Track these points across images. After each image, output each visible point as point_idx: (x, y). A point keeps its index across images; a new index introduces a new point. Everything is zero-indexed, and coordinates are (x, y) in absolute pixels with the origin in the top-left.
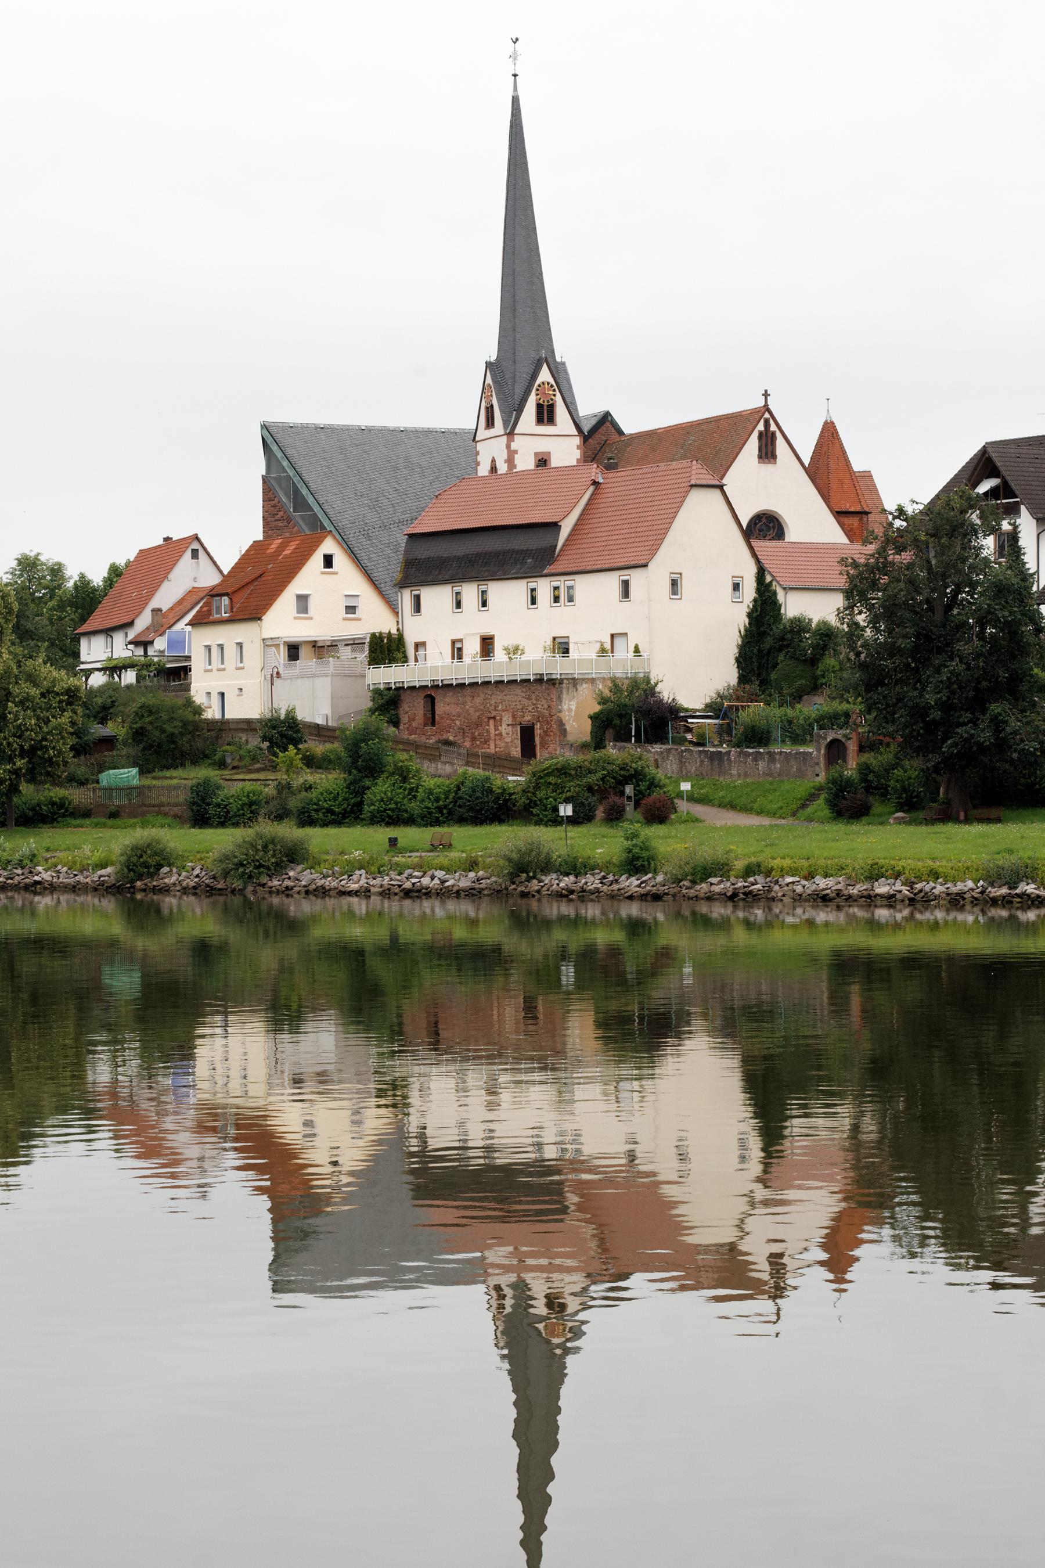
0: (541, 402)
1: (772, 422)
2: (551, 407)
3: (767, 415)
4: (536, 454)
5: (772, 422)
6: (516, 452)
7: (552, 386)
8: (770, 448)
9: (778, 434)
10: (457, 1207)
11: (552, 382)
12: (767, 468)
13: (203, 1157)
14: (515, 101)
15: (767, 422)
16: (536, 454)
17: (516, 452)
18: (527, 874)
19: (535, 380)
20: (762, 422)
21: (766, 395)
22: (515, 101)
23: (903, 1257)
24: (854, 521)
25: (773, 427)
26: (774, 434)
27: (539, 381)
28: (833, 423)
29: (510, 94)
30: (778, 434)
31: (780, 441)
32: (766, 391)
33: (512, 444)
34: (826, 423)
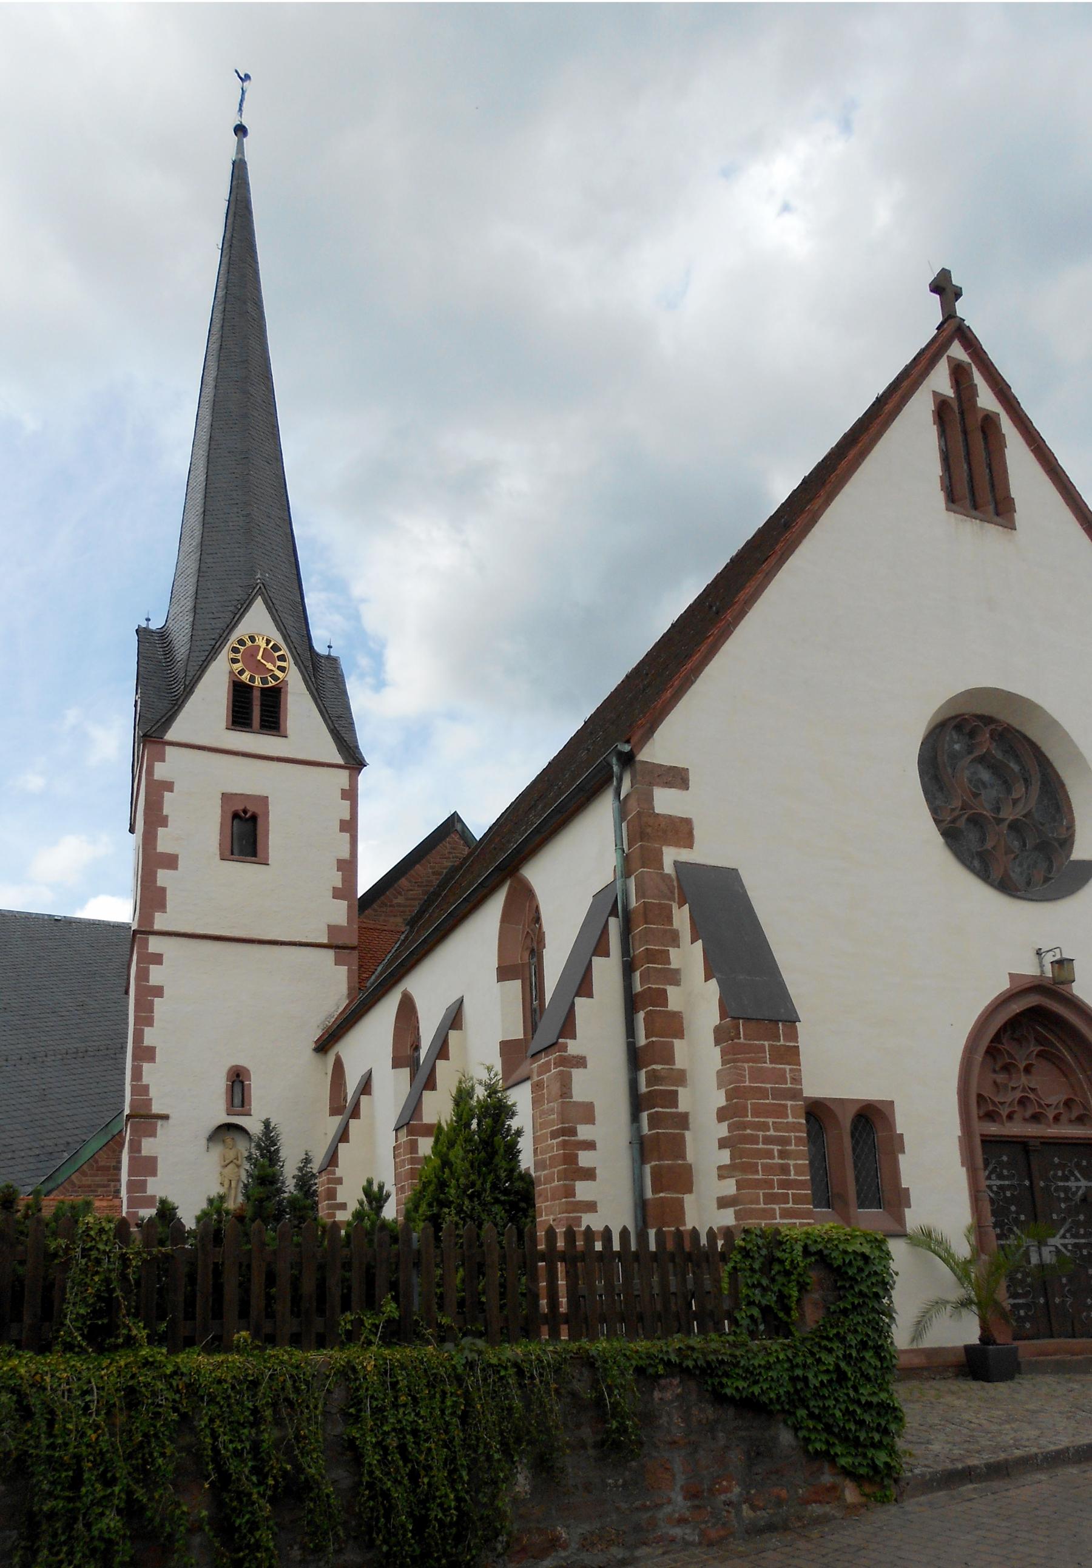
0: (245, 677)
1: (978, 379)
2: (273, 698)
3: (957, 351)
4: (226, 797)
5: (978, 379)
9: (1007, 426)
13: (430, 1399)
14: (239, 169)
15: (959, 373)
16: (226, 797)
18: (411, 1531)
19: (231, 627)
21: (944, 287)
22: (239, 169)
23: (460, 1082)
26: (989, 422)
27: (242, 631)
29: (232, 155)
30: (1007, 426)
31: (1016, 454)
32: (945, 274)
33: (158, 767)
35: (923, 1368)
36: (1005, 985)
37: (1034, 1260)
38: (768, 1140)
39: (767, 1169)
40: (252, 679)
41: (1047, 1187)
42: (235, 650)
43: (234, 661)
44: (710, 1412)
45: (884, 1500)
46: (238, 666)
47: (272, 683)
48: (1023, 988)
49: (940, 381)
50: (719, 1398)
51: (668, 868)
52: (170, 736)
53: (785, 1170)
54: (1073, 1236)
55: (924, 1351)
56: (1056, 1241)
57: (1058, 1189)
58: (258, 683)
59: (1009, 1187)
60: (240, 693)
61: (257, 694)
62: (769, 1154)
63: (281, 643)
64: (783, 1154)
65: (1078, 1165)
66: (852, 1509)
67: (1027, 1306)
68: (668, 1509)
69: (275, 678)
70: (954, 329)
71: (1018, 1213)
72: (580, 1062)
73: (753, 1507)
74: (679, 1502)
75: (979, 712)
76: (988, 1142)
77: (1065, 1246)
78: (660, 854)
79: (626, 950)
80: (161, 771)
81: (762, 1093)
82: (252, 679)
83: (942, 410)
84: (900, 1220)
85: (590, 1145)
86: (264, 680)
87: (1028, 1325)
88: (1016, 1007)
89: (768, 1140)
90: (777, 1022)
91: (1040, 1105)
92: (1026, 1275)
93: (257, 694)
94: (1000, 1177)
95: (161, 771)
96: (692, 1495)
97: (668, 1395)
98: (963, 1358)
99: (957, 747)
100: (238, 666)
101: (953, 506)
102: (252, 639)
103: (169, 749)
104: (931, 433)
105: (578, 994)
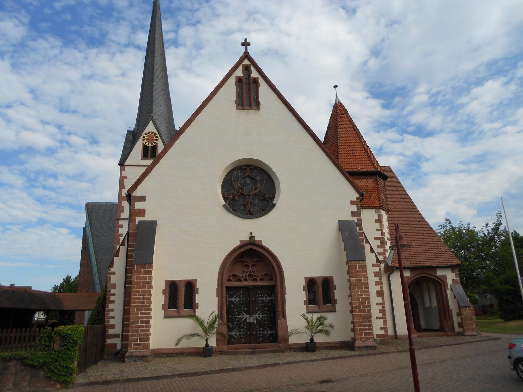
0: (146, 144)
1: (252, 69)
5: (252, 69)
6: (125, 177)
7: (155, 134)
8: (253, 94)
9: (261, 80)
10: (432, 275)
11: (155, 131)
12: (248, 116)
15: (247, 69)
17: (125, 177)
20: (241, 68)
24: (368, 183)
25: (254, 74)
26: (255, 81)
27: (146, 131)
28: (341, 104)
30: (261, 80)
32: (246, 40)
34: (336, 104)
35: (194, 353)
36: (238, 244)
37: (248, 321)
38: (139, 295)
39: (138, 302)
40: (148, 144)
41: (255, 300)
42: (144, 137)
43: (144, 140)
44: (23, 368)
45: (66, 388)
46: (145, 141)
47: (154, 144)
48: (243, 244)
49: (239, 72)
50: (26, 365)
51: (137, 223)
52: (125, 164)
53: (143, 302)
54: (262, 314)
55: (179, 349)
56: (257, 315)
57: (259, 300)
58: (150, 145)
59: (242, 300)
60: (145, 148)
61: (150, 148)
62: (139, 299)
63: (157, 133)
64: (143, 298)
65: (267, 293)
66: (59, 389)
67: (243, 335)
68: (8, 387)
69: (155, 143)
70: (246, 56)
71: (244, 308)
72: (114, 273)
73: (30, 387)
74: (10, 385)
75: (246, 164)
76: (228, 288)
77: (259, 317)
78: (135, 219)
79: (128, 245)
80: (124, 173)
81: (140, 283)
82: (148, 144)
83: (239, 80)
84: (195, 312)
85: (114, 295)
86: (152, 144)
87: (243, 340)
88: (242, 250)
89: (139, 295)
90: (146, 264)
91: (255, 276)
92: (244, 325)
93: (150, 148)
94: (239, 297)
95: (124, 173)
96: (14, 384)
97: (13, 363)
98: (202, 350)
99: (239, 175)
100: (145, 141)
101: (239, 107)
102: (149, 133)
103: (126, 167)
104: (234, 88)
105: (115, 256)
